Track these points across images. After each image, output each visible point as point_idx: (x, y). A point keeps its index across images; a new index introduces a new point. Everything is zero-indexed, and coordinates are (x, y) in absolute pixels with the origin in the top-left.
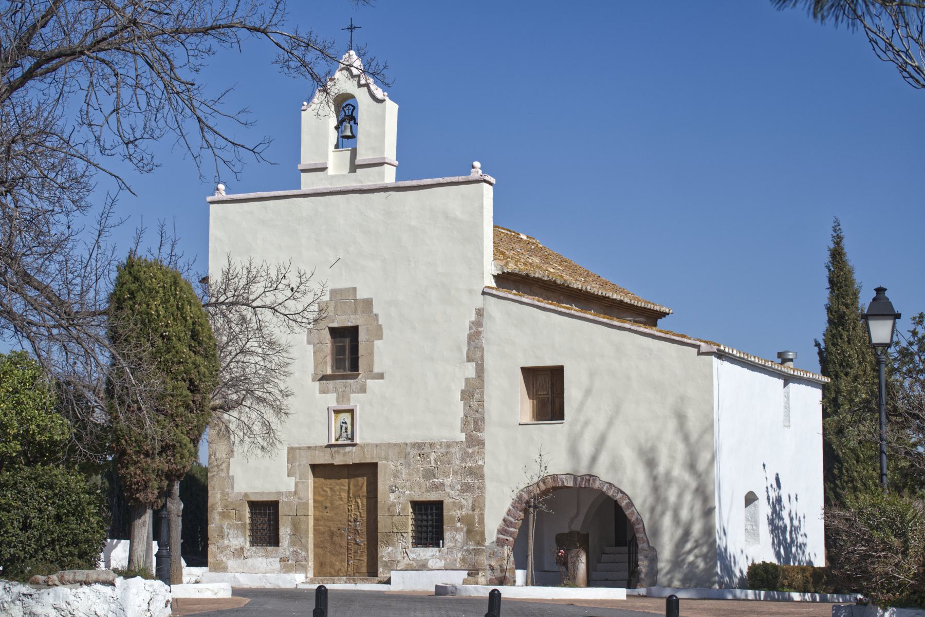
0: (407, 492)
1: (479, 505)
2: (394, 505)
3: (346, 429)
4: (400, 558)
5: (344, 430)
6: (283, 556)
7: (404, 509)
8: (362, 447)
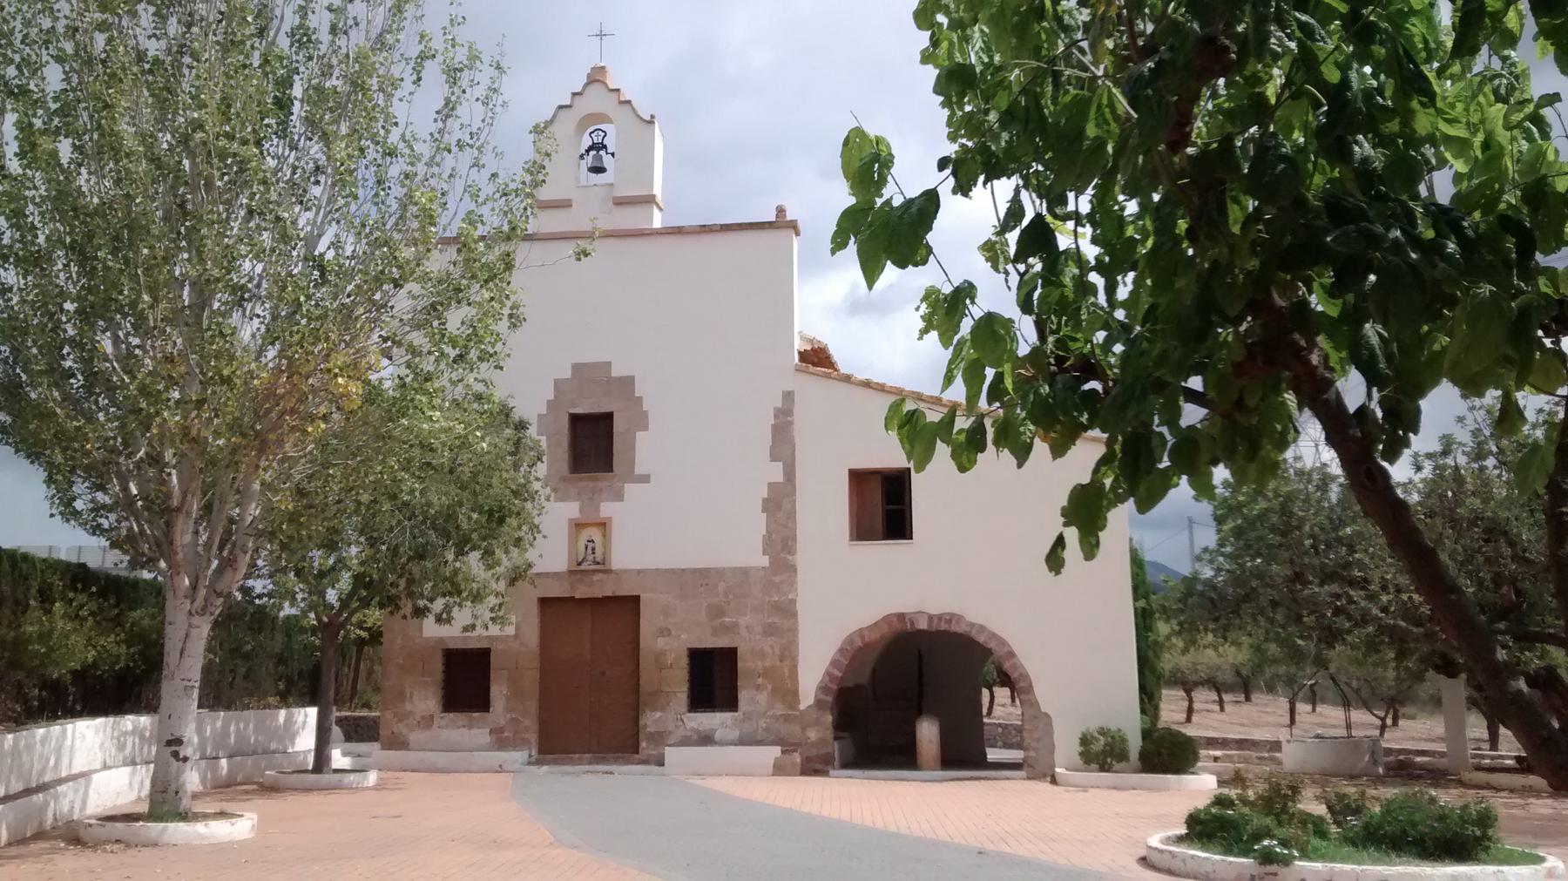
4: (671, 727)
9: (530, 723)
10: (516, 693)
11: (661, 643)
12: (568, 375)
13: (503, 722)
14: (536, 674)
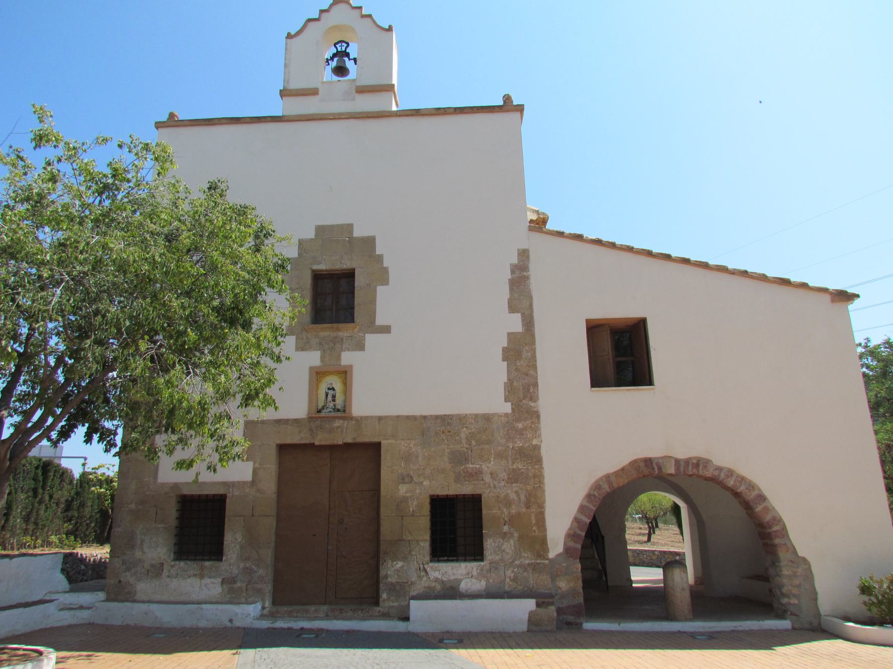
1: (535, 501)
2: (405, 500)
3: (334, 396)
5: (330, 398)
8: (359, 421)
9: (264, 573)
11: (403, 489)
13: (235, 571)
14: (272, 522)
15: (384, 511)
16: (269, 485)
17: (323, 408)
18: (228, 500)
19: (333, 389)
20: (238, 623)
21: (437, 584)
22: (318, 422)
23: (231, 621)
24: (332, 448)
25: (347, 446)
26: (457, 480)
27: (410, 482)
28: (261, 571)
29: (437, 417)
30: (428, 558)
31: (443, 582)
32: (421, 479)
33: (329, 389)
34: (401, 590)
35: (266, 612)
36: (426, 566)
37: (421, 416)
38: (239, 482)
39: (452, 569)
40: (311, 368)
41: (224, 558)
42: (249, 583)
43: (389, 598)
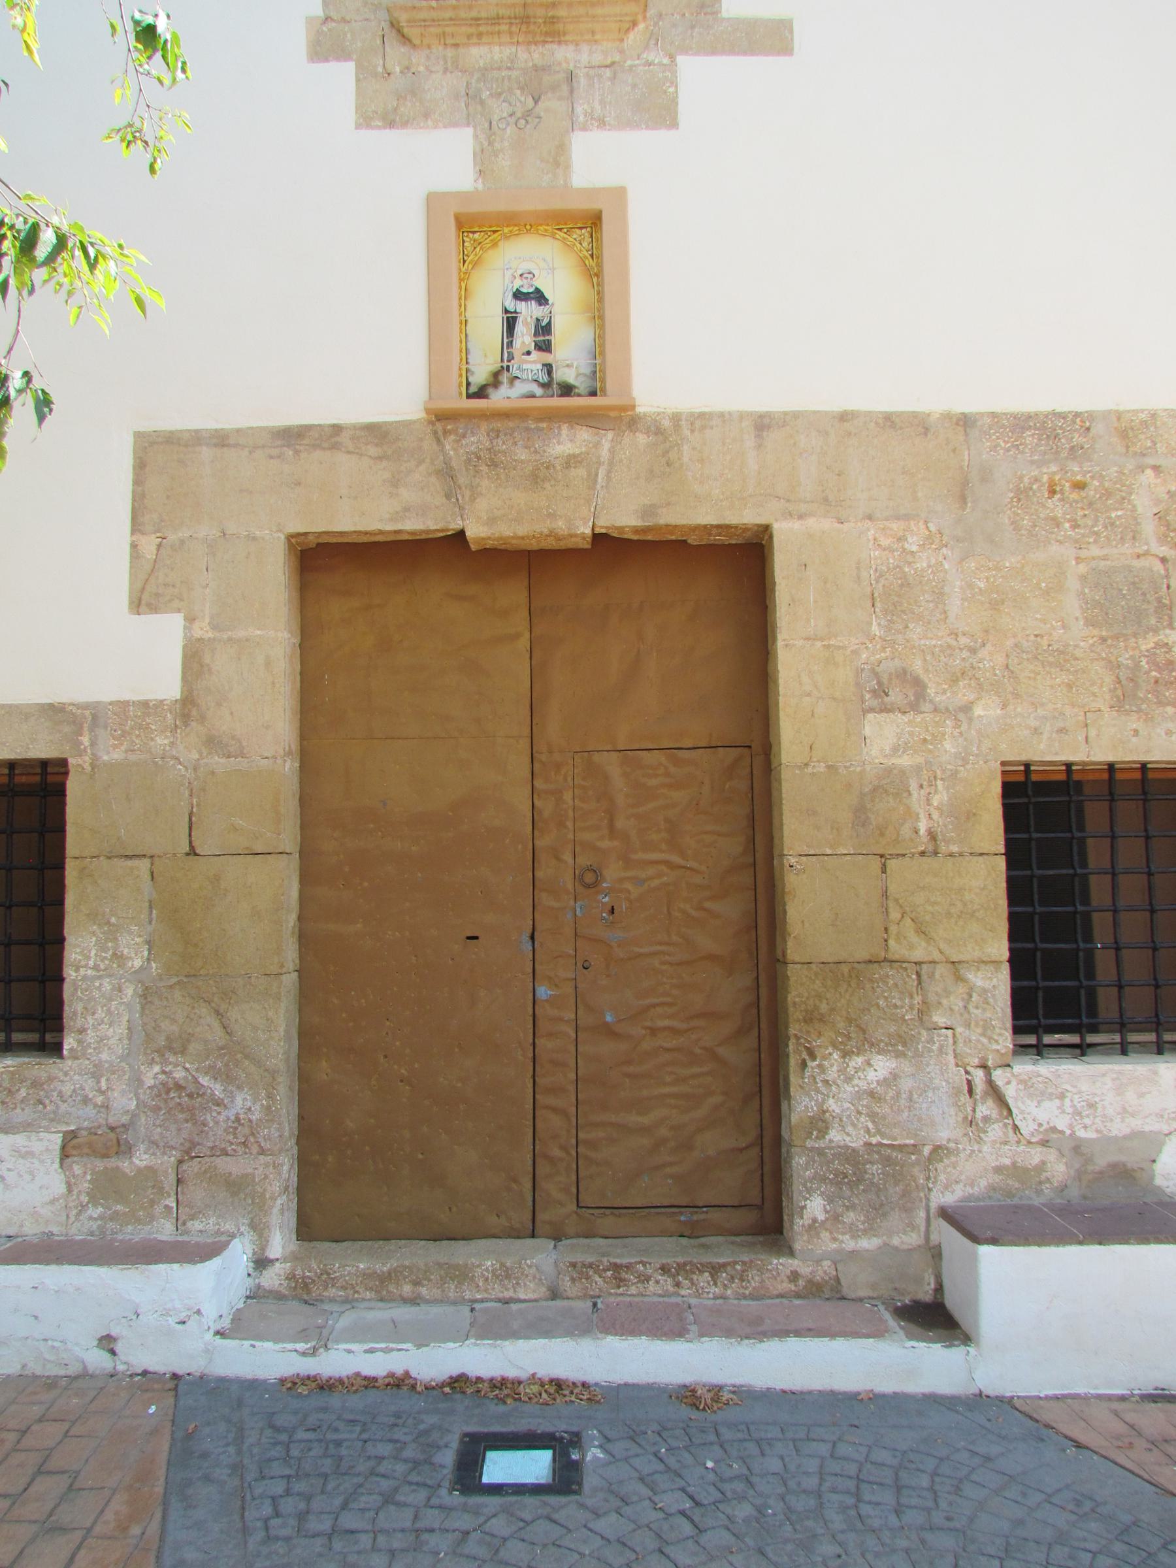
0: (986, 710)
2: (891, 784)
3: (544, 329)
4: (946, 1131)
5: (524, 336)
6: (84, 1117)
7: (964, 815)
8: (666, 433)
9: (259, 1110)
10: (191, 963)
11: (882, 739)
12: (344, 73)
13: (123, 1102)
14: (280, 883)
15: (796, 833)
16: (263, 714)
17: (495, 380)
18: (74, 787)
19: (540, 297)
20: (146, 1354)
21: (1051, 1155)
22: (477, 439)
23: (108, 1342)
24: (533, 564)
25: (607, 546)
26: (1125, 697)
27: (914, 707)
28: (241, 1101)
29: (1021, 423)
30: (1005, 1040)
31: (1078, 1147)
32: (964, 694)
33: (518, 296)
34: (882, 1175)
35: (272, 1278)
36: (999, 1076)
37: (947, 416)
38: (123, 705)
39: (1119, 1090)
40: (433, 201)
41: (69, 1043)
42: (189, 1153)
43: (836, 1218)
